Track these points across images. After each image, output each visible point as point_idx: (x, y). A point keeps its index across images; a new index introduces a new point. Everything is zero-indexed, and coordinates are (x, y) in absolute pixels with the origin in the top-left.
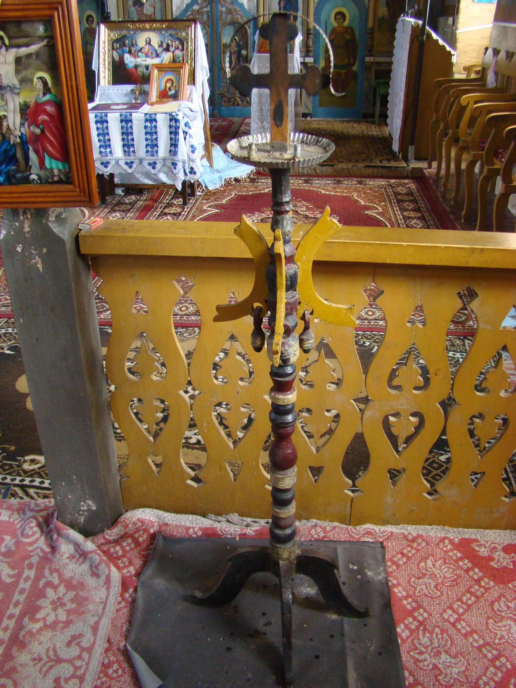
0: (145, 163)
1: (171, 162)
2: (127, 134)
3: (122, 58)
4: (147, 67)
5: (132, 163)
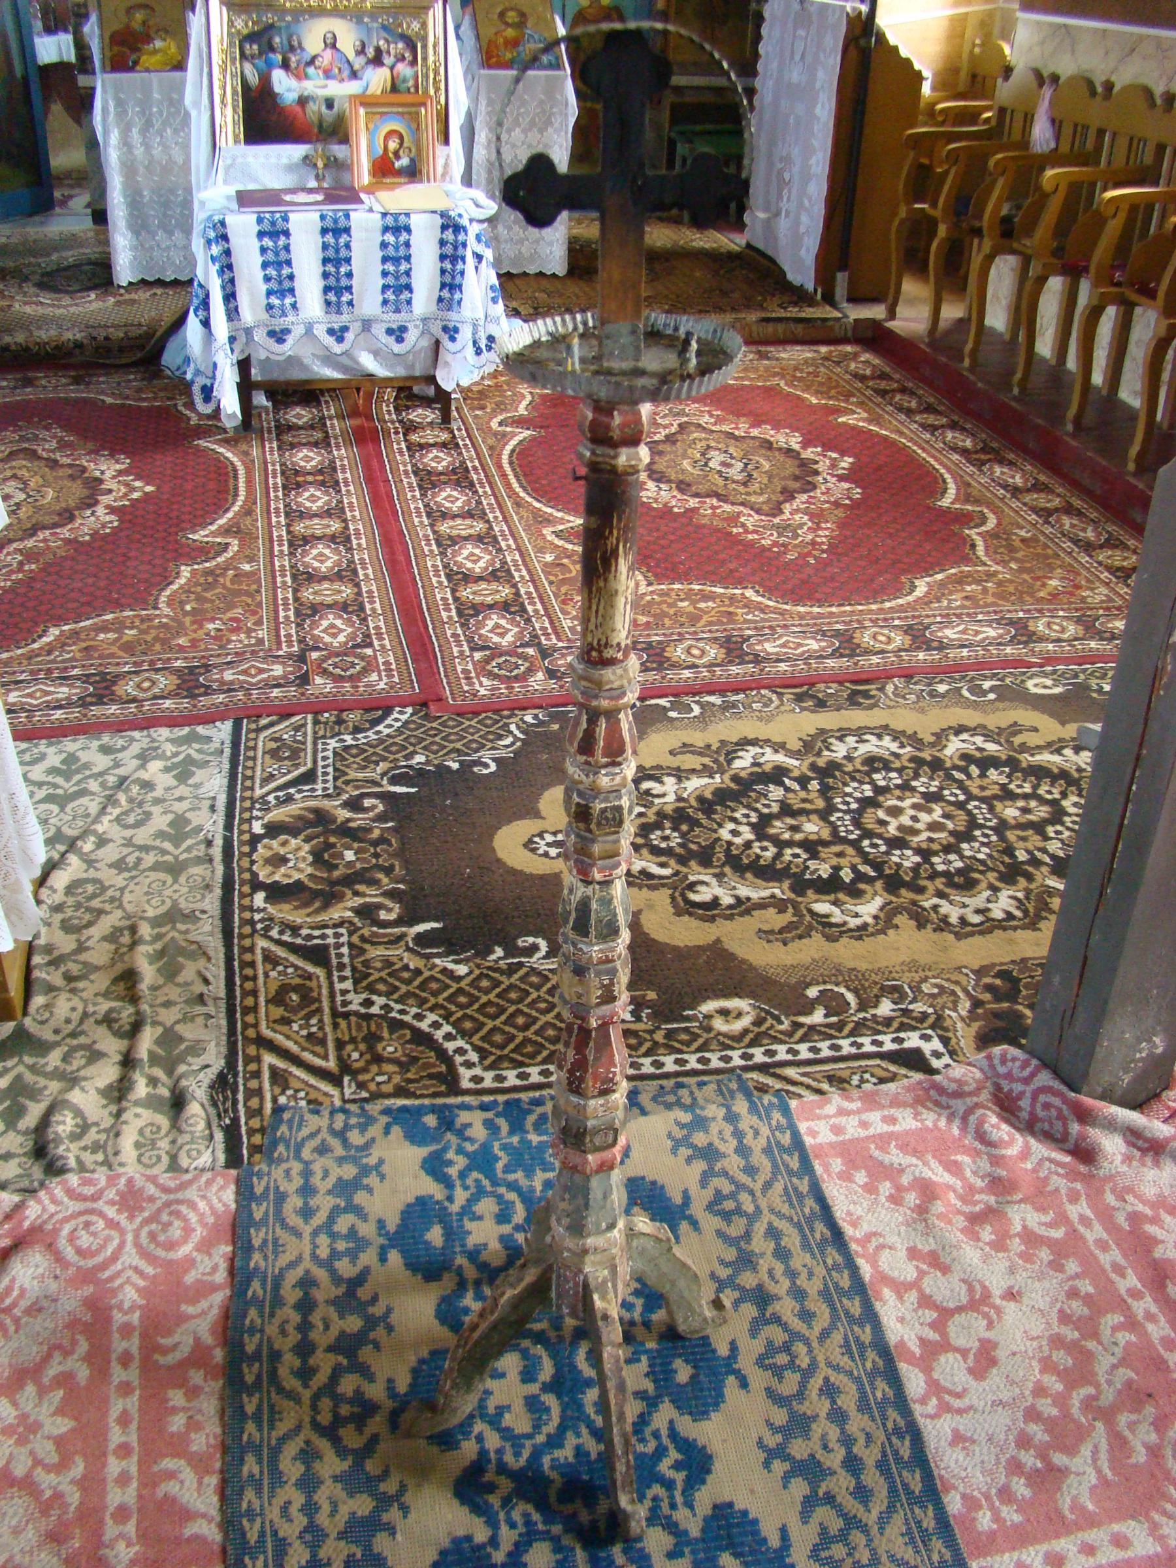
0: (379, 330)
1: (439, 324)
2: (335, 261)
3: (266, 80)
4: (330, 103)
5: (345, 329)
